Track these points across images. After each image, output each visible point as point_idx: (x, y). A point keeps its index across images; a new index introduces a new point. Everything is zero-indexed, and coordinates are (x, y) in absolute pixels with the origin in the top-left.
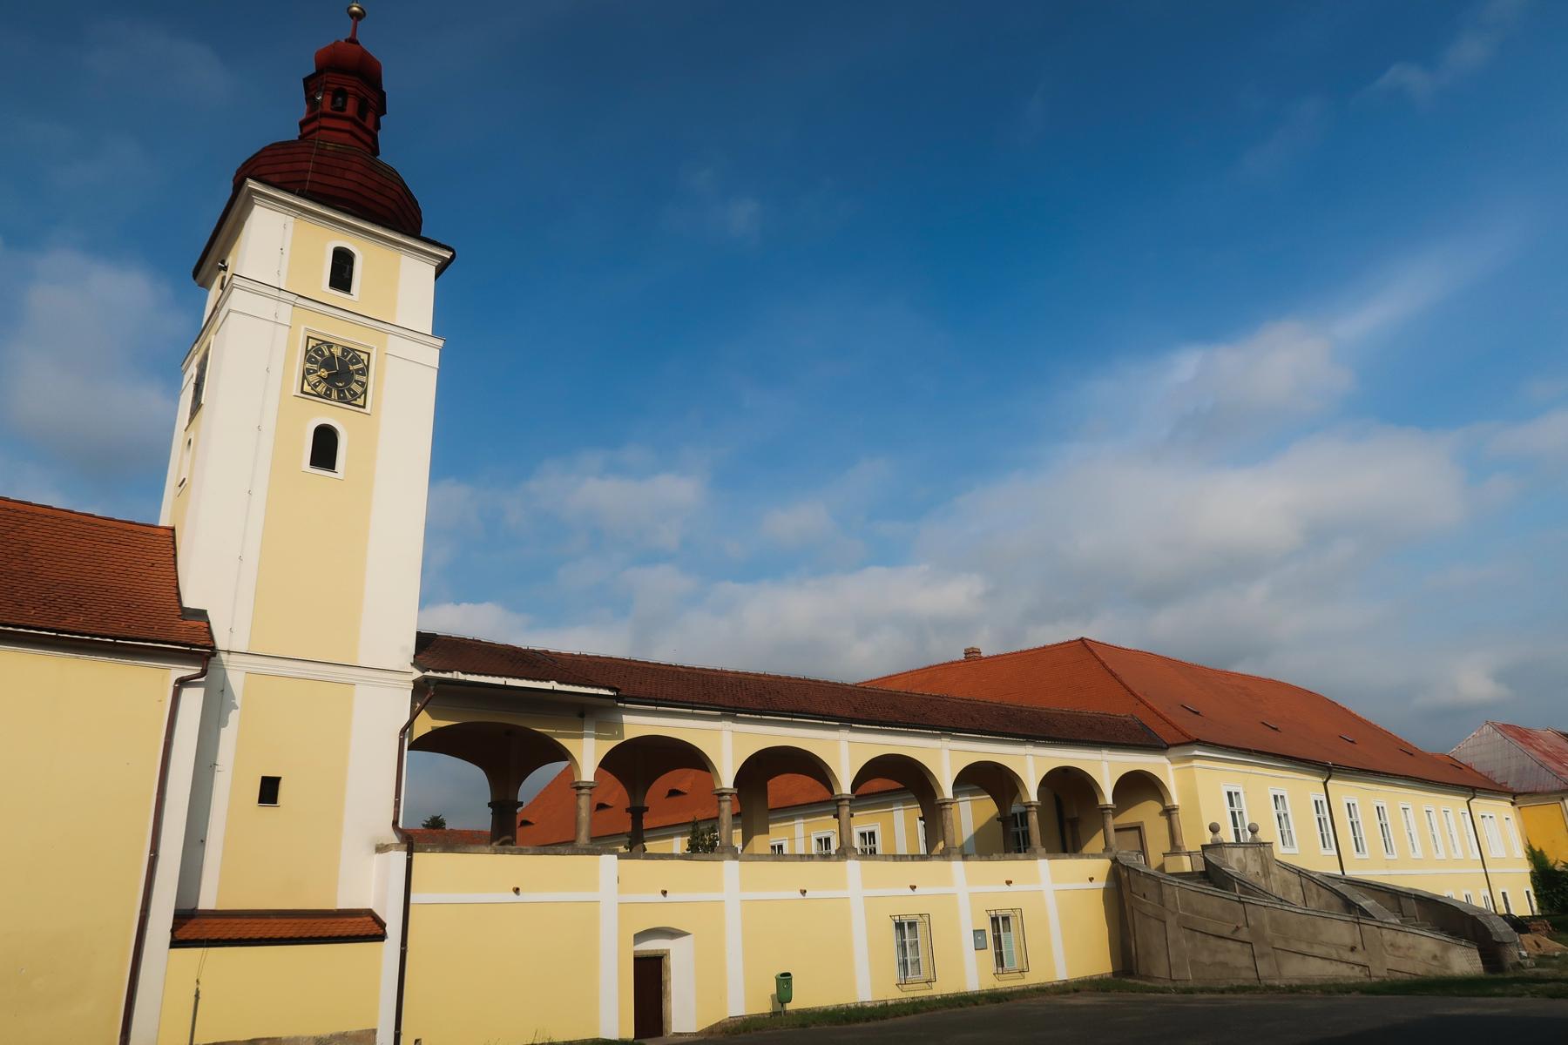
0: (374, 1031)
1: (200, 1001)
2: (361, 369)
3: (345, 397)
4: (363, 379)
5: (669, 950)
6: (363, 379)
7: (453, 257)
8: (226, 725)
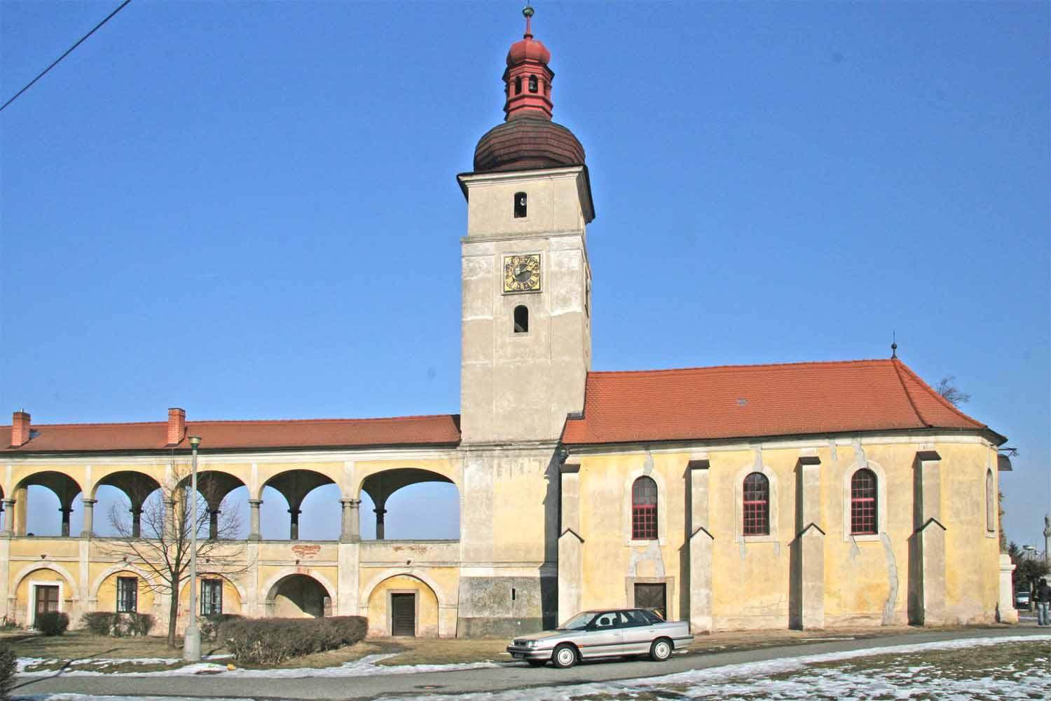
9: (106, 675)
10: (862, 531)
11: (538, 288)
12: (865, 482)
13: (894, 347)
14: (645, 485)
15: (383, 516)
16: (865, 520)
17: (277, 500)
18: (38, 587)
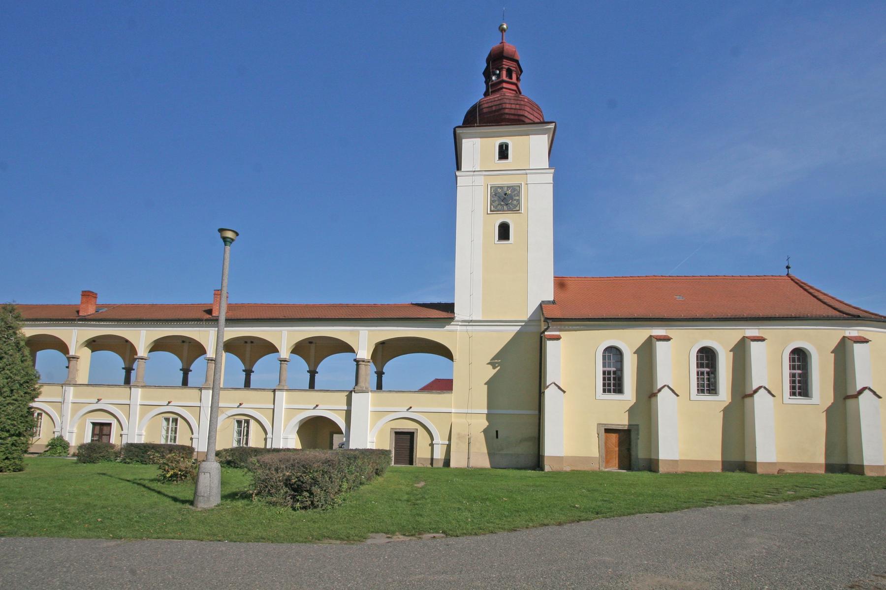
0: (291, 353)
1: (557, 388)
2: (517, 194)
3: (510, 208)
4: (517, 198)
5: (599, 424)
6: (517, 198)
7: (555, 125)
8: (297, 432)
9: (369, 412)
10: (796, 396)
11: (518, 209)
12: (800, 357)
13: (788, 267)
14: (614, 354)
15: (188, 374)
16: (708, 385)
17: (301, 365)
18: (94, 424)
